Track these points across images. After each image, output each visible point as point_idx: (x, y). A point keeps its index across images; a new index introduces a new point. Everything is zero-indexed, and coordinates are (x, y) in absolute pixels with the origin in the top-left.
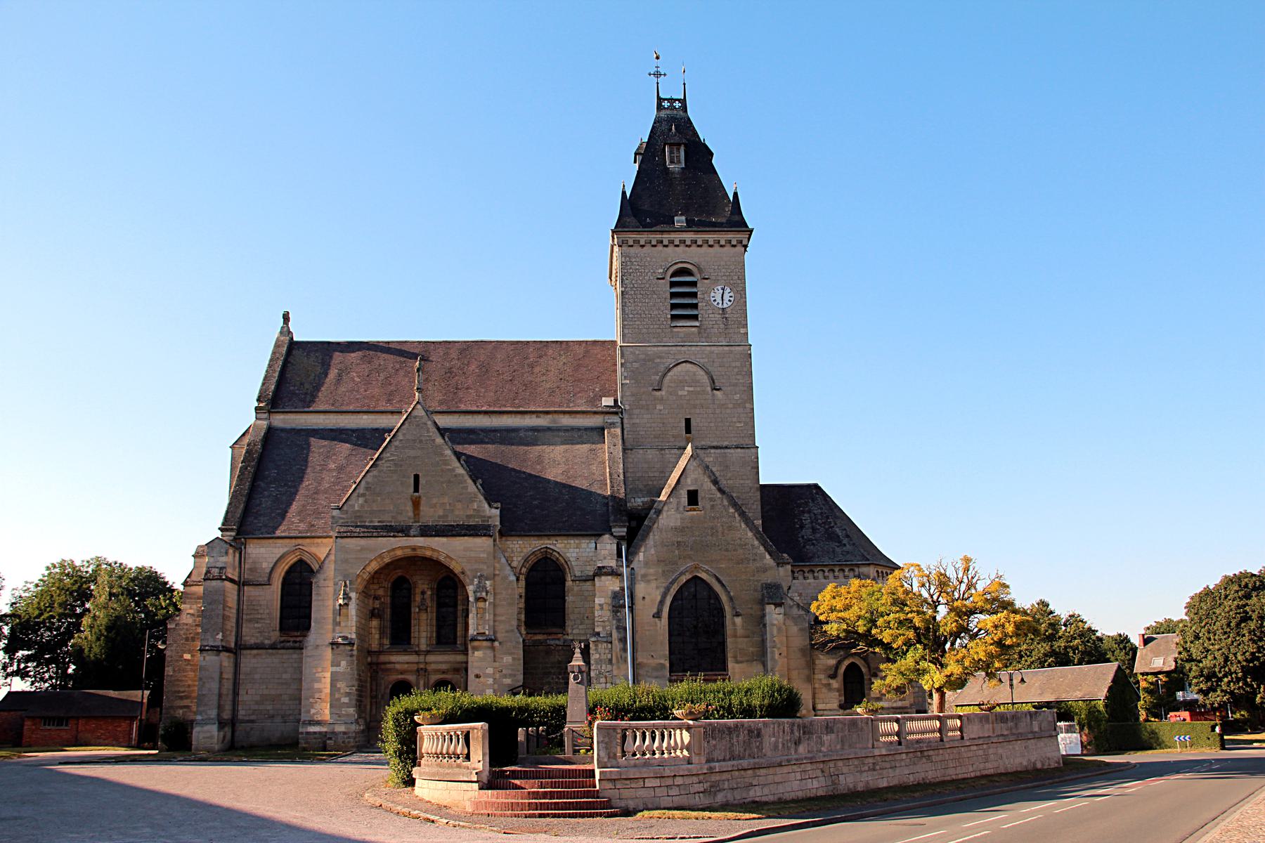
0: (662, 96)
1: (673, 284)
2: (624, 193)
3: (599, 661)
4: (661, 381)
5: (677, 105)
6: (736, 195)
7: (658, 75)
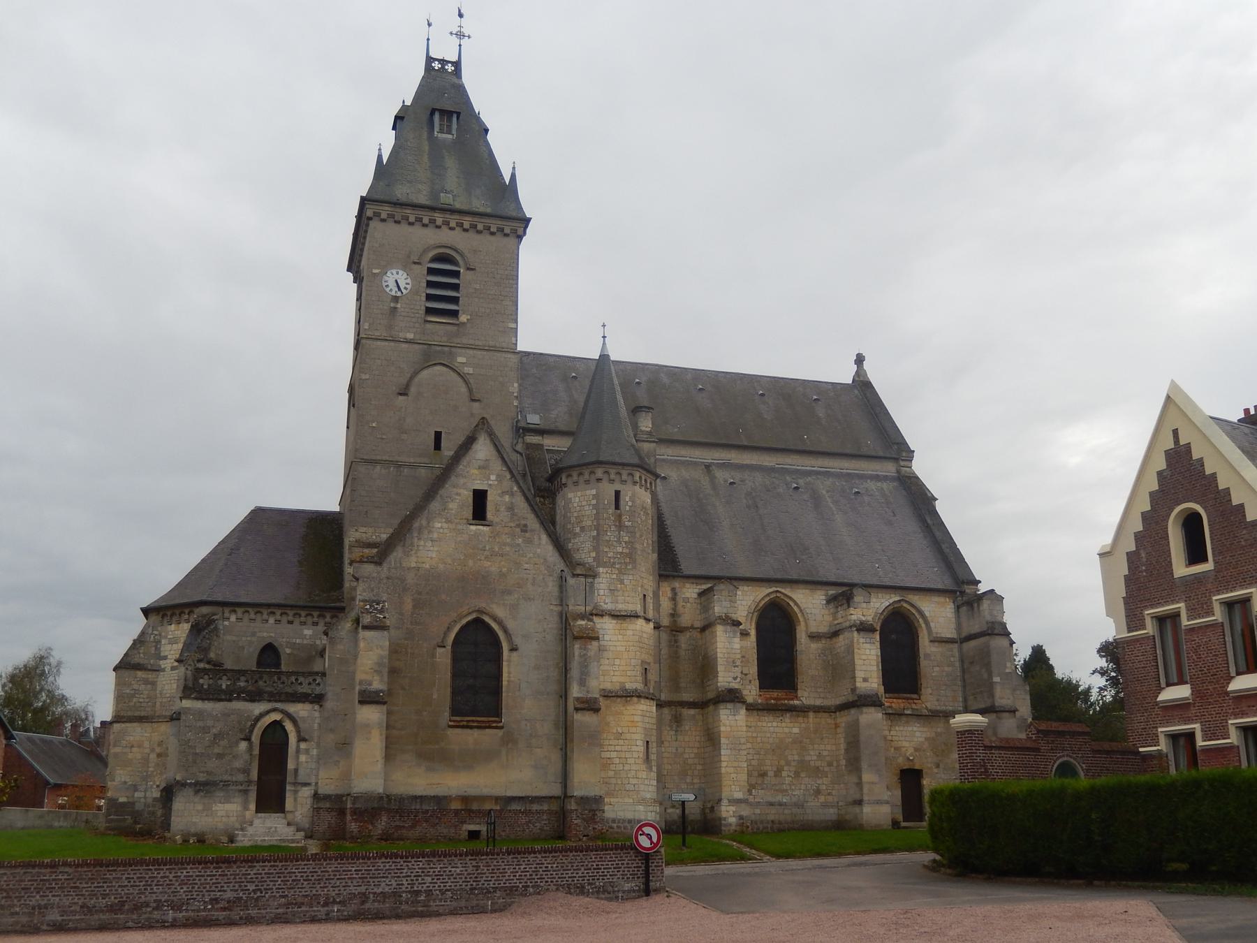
1: (431, 271)
2: (380, 157)
4: (408, 386)
5: (450, 68)
6: (513, 176)
7: (460, 35)
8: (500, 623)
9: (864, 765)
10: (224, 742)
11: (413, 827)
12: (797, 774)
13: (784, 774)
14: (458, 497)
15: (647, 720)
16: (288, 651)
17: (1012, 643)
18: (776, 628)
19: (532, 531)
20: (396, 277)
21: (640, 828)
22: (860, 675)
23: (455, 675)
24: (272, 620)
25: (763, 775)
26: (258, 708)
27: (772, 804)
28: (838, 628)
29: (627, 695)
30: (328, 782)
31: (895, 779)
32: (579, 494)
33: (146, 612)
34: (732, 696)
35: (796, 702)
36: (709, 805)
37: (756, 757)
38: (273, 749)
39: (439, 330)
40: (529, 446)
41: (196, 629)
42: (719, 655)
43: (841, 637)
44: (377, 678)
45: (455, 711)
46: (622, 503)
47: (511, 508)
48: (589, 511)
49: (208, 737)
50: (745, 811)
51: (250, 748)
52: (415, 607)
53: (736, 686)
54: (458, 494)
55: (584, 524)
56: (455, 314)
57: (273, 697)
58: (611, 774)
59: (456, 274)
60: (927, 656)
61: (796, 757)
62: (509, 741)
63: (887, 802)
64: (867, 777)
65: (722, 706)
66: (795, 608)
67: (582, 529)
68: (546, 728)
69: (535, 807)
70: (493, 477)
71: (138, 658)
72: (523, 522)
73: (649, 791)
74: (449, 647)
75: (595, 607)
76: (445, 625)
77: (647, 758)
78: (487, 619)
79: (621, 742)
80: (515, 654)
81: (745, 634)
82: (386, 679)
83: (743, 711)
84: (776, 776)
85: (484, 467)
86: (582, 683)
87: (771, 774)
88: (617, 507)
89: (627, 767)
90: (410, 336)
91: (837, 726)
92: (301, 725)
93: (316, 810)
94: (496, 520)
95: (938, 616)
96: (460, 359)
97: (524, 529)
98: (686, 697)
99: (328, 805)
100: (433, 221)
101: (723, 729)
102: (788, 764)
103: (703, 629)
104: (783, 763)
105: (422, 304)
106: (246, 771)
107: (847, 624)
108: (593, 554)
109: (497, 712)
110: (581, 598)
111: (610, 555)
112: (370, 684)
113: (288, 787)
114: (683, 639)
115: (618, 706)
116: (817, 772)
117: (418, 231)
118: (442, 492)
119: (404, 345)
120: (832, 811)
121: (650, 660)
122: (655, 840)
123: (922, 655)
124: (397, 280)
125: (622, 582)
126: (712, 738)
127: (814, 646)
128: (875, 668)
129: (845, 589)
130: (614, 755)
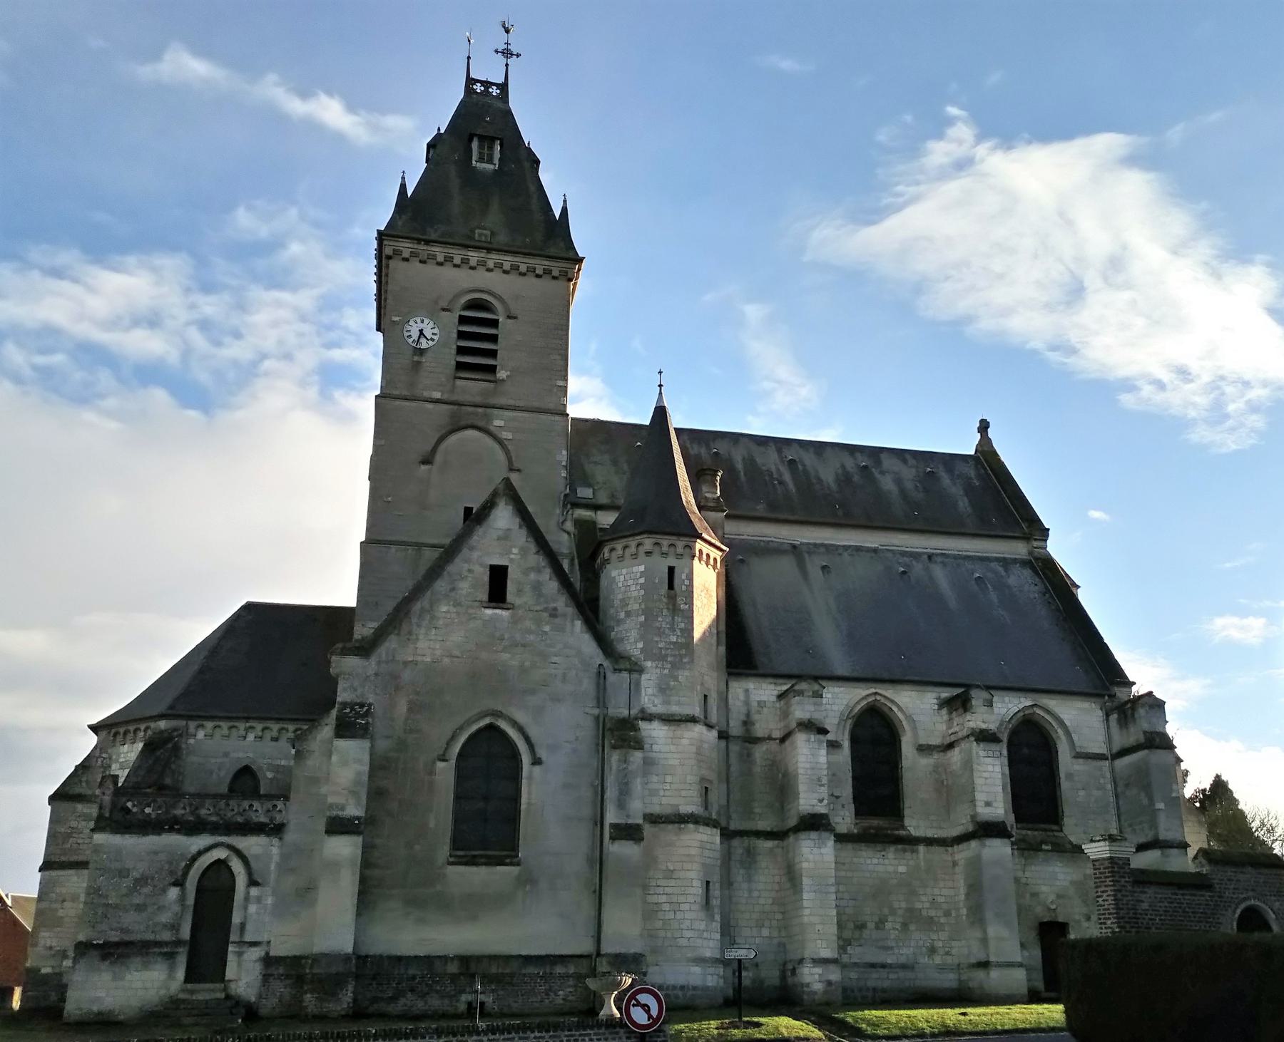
0: (473, 75)
1: (463, 320)
2: (403, 187)
3: (975, 865)
5: (494, 91)
6: (564, 211)
7: (507, 53)
8: (521, 730)
9: (989, 915)
10: (146, 890)
11: (394, 999)
12: (905, 926)
13: (888, 925)
14: (470, 573)
15: (707, 853)
16: (270, 775)
17: (1179, 760)
18: (875, 740)
19: (564, 615)
20: (421, 326)
21: (633, 997)
22: (980, 797)
23: (458, 798)
24: (251, 737)
25: (861, 927)
26: (203, 841)
27: (873, 966)
28: (953, 738)
29: (681, 820)
30: (286, 939)
31: (1033, 936)
32: (624, 571)
33: (95, 728)
34: (814, 823)
35: (903, 833)
36: (790, 967)
37: (852, 903)
38: (214, 897)
39: (471, 388)
40: (579, 523)
41: (150, 747)
42: (801, 771)
43: (957, 750)
44: (352, 801)
45: (456, 843)
46: (676, 582)
47: (537, 587)
48: (636, 592)
49: (127, 883)
50: (835, 975)
51: (182, 898)
52: (410, 710)
53: (823, 811)
54: (470, 571)
55: (629, 608)
56: (492, 369)
57: (214, 829)
58: (659, 924)
59: (495, 323)
60: (1070, 776)
61: (903, 905)
62: (527, 881)
63: (1020, 965)
64: (992, 931)
65: (803, 835)
66: (900, 715)
67: (628, 614)
68: (576, 863)
69: (559, 970)
70: (515, 551)
71: (81, 789)
72: (553, 605)
73: (710, 948)
74: (453, 762)
75: (643, 710)
76: (448, 732)
77: (707, 904)
78: (503, 725)
79: (672, 883)
80: (537, 769)
81: (833, 745)
82: (364, 801)
83: (831, 843)
84: (877, 928)
85: (505, 536)
86: (621, 805)
87: (871, 925)
88: (671, 586)
89: (679, 915)
90: (437, 395)
91: (955, 864)
92: (253, 864)
93: (266, 978)
94: (518, 602)
95: (1079, 721)
96: (498, 423)
97: (554, 613)
98: (763, 825)
99: (281, 971)
100: (465, 261)
101: (805, 865)
102: (893, 912)
103: (783, 740)
104: (886, 911)
105: (451, 358)
106: (175, 927)
107: (965, 733)
108: (640, 645)
109: (515, 848)
110: (623, 698)
111: (661, 645)
112: (343, 809)
113: (231, 948)
114: (759, 752)
115: (668, 833)
116: (930, 924)
117: (448, 272)
118: (451, 568)
119: (430, 406)
120: (952, 976)
121: (712, 776)
122: (654, 1013)
123: (1062, 775)
124: (425, 329)
125: (676, 679)
126: (792, 876)
127: (926, 762)
128: (1000, 789)
129: (960, 690)
130: (663, 899)
